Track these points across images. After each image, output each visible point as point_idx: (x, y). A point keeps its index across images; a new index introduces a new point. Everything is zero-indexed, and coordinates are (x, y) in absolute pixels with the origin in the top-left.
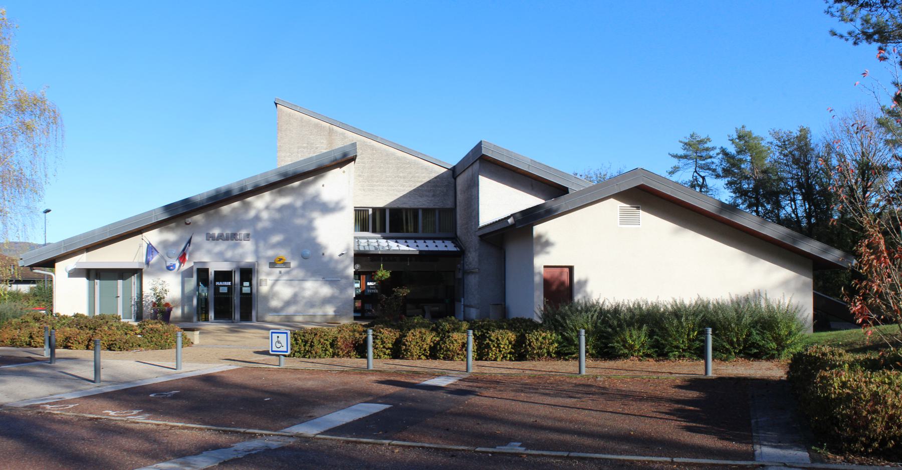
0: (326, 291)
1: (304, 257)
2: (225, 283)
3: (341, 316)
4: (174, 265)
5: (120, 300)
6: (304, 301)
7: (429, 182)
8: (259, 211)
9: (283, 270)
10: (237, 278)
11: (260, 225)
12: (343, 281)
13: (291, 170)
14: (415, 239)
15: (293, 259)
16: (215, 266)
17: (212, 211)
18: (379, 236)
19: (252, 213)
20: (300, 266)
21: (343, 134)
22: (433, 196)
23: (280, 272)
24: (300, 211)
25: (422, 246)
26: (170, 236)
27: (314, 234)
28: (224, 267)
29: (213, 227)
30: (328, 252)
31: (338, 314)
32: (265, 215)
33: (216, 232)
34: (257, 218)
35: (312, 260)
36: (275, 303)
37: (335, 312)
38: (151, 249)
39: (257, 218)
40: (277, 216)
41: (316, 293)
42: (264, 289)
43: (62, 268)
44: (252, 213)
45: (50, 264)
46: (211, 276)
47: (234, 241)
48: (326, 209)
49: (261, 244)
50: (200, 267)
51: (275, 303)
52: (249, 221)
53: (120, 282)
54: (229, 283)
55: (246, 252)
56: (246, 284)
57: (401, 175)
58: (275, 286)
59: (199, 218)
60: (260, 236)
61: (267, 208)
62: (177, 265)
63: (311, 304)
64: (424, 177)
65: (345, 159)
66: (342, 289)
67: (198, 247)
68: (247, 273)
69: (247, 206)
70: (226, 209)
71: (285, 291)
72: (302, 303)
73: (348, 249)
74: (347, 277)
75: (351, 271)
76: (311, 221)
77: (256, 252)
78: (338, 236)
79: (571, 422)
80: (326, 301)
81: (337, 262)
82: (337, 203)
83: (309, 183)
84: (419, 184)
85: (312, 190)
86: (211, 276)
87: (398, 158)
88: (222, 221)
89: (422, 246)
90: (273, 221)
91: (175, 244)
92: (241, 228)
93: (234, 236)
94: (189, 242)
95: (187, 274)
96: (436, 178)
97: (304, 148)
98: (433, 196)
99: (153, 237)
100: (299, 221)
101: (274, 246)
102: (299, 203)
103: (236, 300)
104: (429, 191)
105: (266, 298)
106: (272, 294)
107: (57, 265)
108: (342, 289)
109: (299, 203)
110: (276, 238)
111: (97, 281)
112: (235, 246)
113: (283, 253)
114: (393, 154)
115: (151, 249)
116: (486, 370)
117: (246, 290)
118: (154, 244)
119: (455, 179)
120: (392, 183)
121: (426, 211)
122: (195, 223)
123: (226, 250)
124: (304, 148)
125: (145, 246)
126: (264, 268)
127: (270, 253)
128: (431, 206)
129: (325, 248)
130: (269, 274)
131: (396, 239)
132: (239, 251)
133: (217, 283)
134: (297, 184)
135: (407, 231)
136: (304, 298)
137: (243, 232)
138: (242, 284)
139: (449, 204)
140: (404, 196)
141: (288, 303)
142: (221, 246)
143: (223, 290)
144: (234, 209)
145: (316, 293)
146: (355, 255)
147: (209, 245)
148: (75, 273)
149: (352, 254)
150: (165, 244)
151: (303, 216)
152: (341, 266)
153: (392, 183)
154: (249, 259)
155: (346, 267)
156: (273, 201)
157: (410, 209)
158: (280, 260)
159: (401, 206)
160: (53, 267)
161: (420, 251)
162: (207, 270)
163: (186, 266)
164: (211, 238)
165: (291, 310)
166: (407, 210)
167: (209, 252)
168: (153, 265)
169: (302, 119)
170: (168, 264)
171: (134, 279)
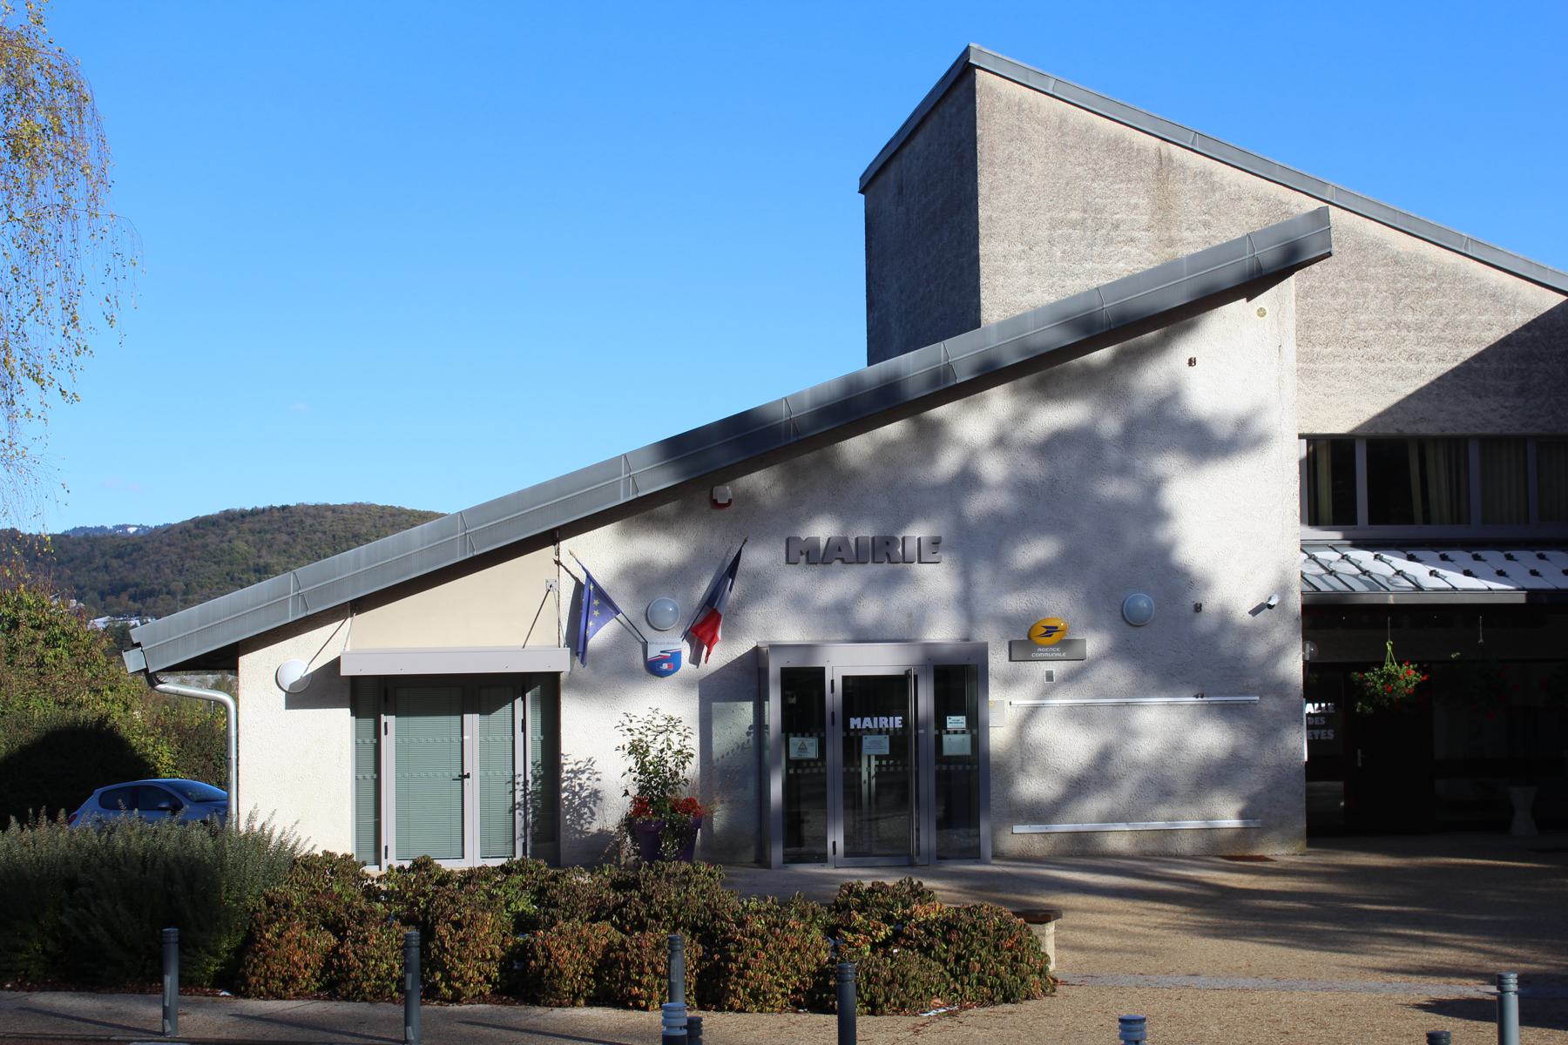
0: (1211, 739)
1: (1130, 620)
2: (884, 722)
3: (1264, 830)
4: (676, 656)
5: (472, 787)
6: (1137, 776)
8: (973, 454)
9: (1057, 668)
10: (924, 700)
11: (978, 505)
12: (1270, 704)
13: (1109, 304)
14: (1505, 545)
15: (1093, 625)
16: (845, 661)
17: (808, 458)
18: (1335, 535)
19: (948, 463)
20: (1121, 651)
21: (1205, 175)
23: (1049, 676)
24: (1113, 456)
25: (1556, 573)
26: (662, 549)
27: (1163, 535)
28: (879, 661)
30: (1213, 600)
31: (1258, 817)
32: (993, 468)
33: (822, 530)
34: (967, 480)
35: (1159, 625)
36: (1033, 787)
37: (1242, 815)
38: (589, 599)
39: (967, 480)
40: (1034, 469)
41: (1177, 747)
42: (999, 734)
43: (263, 676)
44: (948, 463)
45: (223, 661)
46: (834, 697)
47: (886, 566)
48: (1208, 443)
49: (983, 576)
50: (793, 661)
51: (1033, 787)
52: (937, 489)
53: (473, 721)
54: (897, 721)
55: (933, 603)
56: (956, 722)
57: (1409, 318)
58: (1038, 724)
59: (760, 481)
60: (977, 544)
61: (1001, 442)
62: (686, 650)
63: (1159, 787)
64: (1489, 326)
65: (1285, 260)
66: (1268, 731)
67: (761, 589)
68: (959, 680)
69: (931, 437)
70: (857, 448)
71: (1067, 745)
73: (1283, 590)
74: (1279, 688)
75: (1293, 666)
76: (1154, 486)
77: (966, 603)
78: (1245, 540)
80: (1215, 776)
81: (1246, 633)
82: (1243, 423)
83: (1162, 345)
84: (1469, 351)
85: (1154, 376)
86: (834, 697)
87: (1397, 260)
88: (841, 490)
89: (1556, 573)
90: (1022, 487)
91: (677, 576)
93: (883, 550)
94: (732, 570)
95: (717, 692)
96: (1527, 327)
97: (1074, 225)
99: (600, 553)
100: (1113, 489)
101: (1041, 575)
102: (1110, 425)
103: (927, 784)
105: (1006, 772)
106: (1025, 752)
107: (245, 661)
108: (1268, 731)
109: (1110, 425)
110: (1036, 551)
111: (388, 720)
112: (893, 582)
113: (1056, 605)
114: (1379, 245)
115: (589, 599)
117: (956, 742)
118: (601, 579)
120: (1377, 349)
121: (1489, 443)
122: (749, 498)
123: (859, 597)
124: (1074, 225)
126: (998, 661)
127: (1015, 603)
128: (1514, 427)
129: (1206, 585)
130: (1010, 681)
131: (1409, 547)
132: (905, 598)
133: (855, 722)
134: (1101, 355)
135: (1427, 521)
136: (1135, 765)
137: (917, 532)
138: (941, 724)
140: (1420, 394)
141: (1078, 787)
142: (838, 585)
144: (886, 451)
145: (1177, 747)
146: (1306, 608)
147: (797, 579)
149: (1296, 603)
150: (643, 579)
151: (1124, 470)
152: (1259, 649)
153: (1377, 349)
154: (943, 632)
155: (1278, 652)
156: (1020, 418)
157: (1435, 440)
158: (1050, 631)
159: (1410, 430)
160: (234, 668)
161: (1532, 594)
162: (821, 671)
163: (721, 655)
165: (1088, 815)
166: (1422, 442)
167: (799, 603)
168: (602, 653)
169: (1063, 120)
170: (653, 653)
171: (525, 710)
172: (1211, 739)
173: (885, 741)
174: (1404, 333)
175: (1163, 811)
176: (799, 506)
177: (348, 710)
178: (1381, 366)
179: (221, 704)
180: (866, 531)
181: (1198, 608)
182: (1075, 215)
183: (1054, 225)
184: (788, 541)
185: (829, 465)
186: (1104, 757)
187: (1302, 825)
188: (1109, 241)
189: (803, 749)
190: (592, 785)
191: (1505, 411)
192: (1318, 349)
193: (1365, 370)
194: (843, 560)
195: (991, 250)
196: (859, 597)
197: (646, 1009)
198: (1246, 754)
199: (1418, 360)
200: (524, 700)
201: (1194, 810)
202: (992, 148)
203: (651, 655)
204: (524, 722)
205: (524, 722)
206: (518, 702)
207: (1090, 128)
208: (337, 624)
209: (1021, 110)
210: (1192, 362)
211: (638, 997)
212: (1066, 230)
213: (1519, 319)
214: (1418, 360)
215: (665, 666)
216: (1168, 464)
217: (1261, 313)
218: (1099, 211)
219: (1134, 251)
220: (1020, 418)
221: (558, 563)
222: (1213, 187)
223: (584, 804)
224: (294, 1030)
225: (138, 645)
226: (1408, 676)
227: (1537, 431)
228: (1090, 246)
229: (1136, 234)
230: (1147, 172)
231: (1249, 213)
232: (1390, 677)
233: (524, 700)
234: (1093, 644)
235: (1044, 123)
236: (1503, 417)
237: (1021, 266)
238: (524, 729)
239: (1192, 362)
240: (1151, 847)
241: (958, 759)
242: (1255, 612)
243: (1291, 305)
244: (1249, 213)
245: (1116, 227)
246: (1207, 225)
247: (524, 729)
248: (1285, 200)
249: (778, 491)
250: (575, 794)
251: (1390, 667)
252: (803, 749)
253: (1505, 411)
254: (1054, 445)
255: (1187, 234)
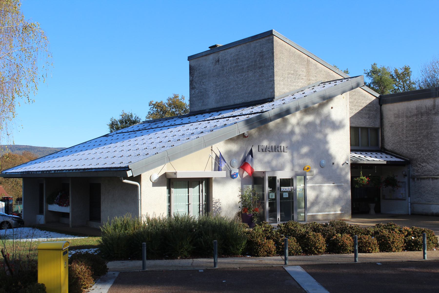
0: (336, 193)
1: (321, 166)
6: (323, 202)
7: (366, 107)
8: (293, 126)
11: (296, 138)
15: (315, 167)
19: (289, 128)
20: (320, 173)
22: (369, 118)
24: (318, 128)
26: (234, 147)
27: (327, 147)
29: (263, 140)
33: (265, 143)
34: (292, 133)
37: (341, 211)
38: (219, 159)
39: (292, 133)
40: (304, 131)
44: (289, 128)
46: (278, 184)
61: (298, 124)
63: (327, 205)
69: (285, 122)
72: (321, 205)
73: (348, 160)
76: (326, 135)
78: (340, 147)
79: (182, 267)
80: (336, 201)
81: (342, 169)
82: (341, 122)
84: (361, 108)
90: (303, 135)
91: (236, 154)
92: (281, 142)
93: (276, 149)
95: (244, 182)
96: (370, 104)
97: (292, 74)
98: (369, 118)
100: (319, 136)
102: (318, 121)
104: (366, 114)
109: (318, 121)
112: (279, 156)
116: (264, 262)
119: (381, 105)
123: (272, 160)
124: (292, 74)
125: (214, 157)
127: (301, 161)
129: (335, 158)
137: (283, 145)
139: (378, 125)
143: (286, 195)
144: (277, 125)
145: (330, 195)
148: (156, 184)
149: (349, 162)
150: (230, 154)
151: (320, 132)
155: (347, 173)
161: (387, 162)
164: (265, 150)
170: (232, 173)
172: (336, 193)
173: (287, 194)
175: (327, 210)
176: (260, 138)
177: (166, 187)
179: (137, 186)
180: (273, 144)
181: (333, 164)
182: (292, 72)
183: (289, 74)
184: (259, 146)
185: (266, 128)
186: (317, 197)
187: (351, 213)
188: (299, 79)
189: (272, 196)
190: (219, 206)
194: (269, 151)
195: (277, 79)
196: (272, 160)
197: (372, 252)
198: (341, 196)
200: (202, 185)
201: (332, 209)
202: (277, 55)
203: (232, 173)
204: (202, 190)
205: (202, 190)
206: (201, 185)
207: (295, 52)
208: (162, 166)
209: (282, 46)
210: (332, 108)
211: (370, 250)
212: (290, 75)
213: (368, 102)
215: (235, 176)
216: (328, 131)
217: (343, 98)
218: (297, 71)
219: (303, 81)
220: (302, 119)
221: (212, 150)
222: (317, 68)
223: (217, 210)
224: (306, 262)
225: (131, 169)
226: (365, 179)
227: (371, 127)
228: (295, 79)
229: (303, 77)
230: (305, 63)
231: (323, 74)
232: (362, 179)
233: (202, 185)
234: (315, 171)
235: (286, 50)
237: (282, 83)
238: (202, 192)
239: (332, 108)
240: (325, 218)
241: (286, 198)
242: (343, 165)
243: (348, 97)
244: (323, 74)
245: (300, 75)
246: (316, 76)
247: (202, 192)
249: (257, 133)
250: (216, 208)
251: (362, 177)
252: (272, 196)
254: (309, 125)
255: (312, 78)
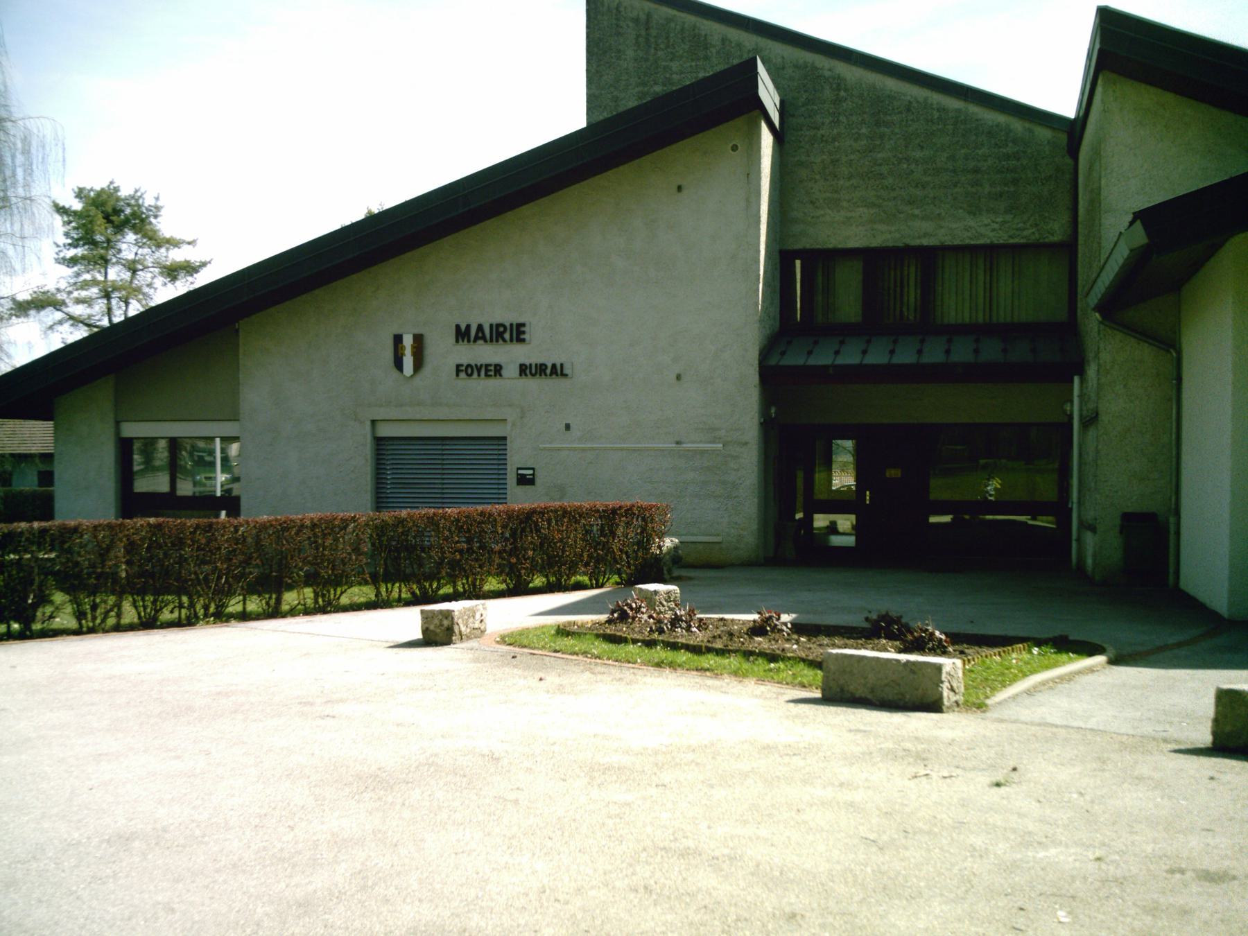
57: (918, 154)
174: (913, 167)
178: (893, 194)
191: (996, 226)
192: (841, 182)
193: (879, 197)
199: (924, 187)
214: (924, 187)
236: (993, 230)
248: (820, 66)
253: (996, 226)
